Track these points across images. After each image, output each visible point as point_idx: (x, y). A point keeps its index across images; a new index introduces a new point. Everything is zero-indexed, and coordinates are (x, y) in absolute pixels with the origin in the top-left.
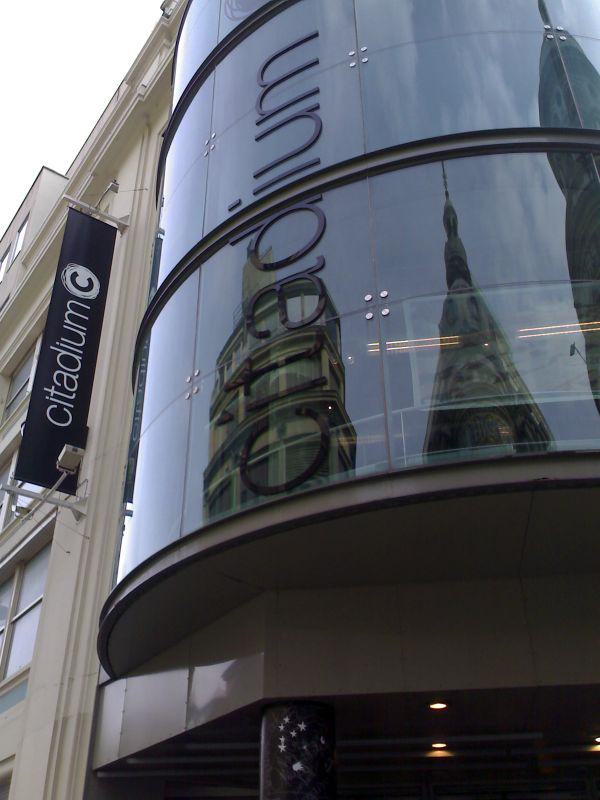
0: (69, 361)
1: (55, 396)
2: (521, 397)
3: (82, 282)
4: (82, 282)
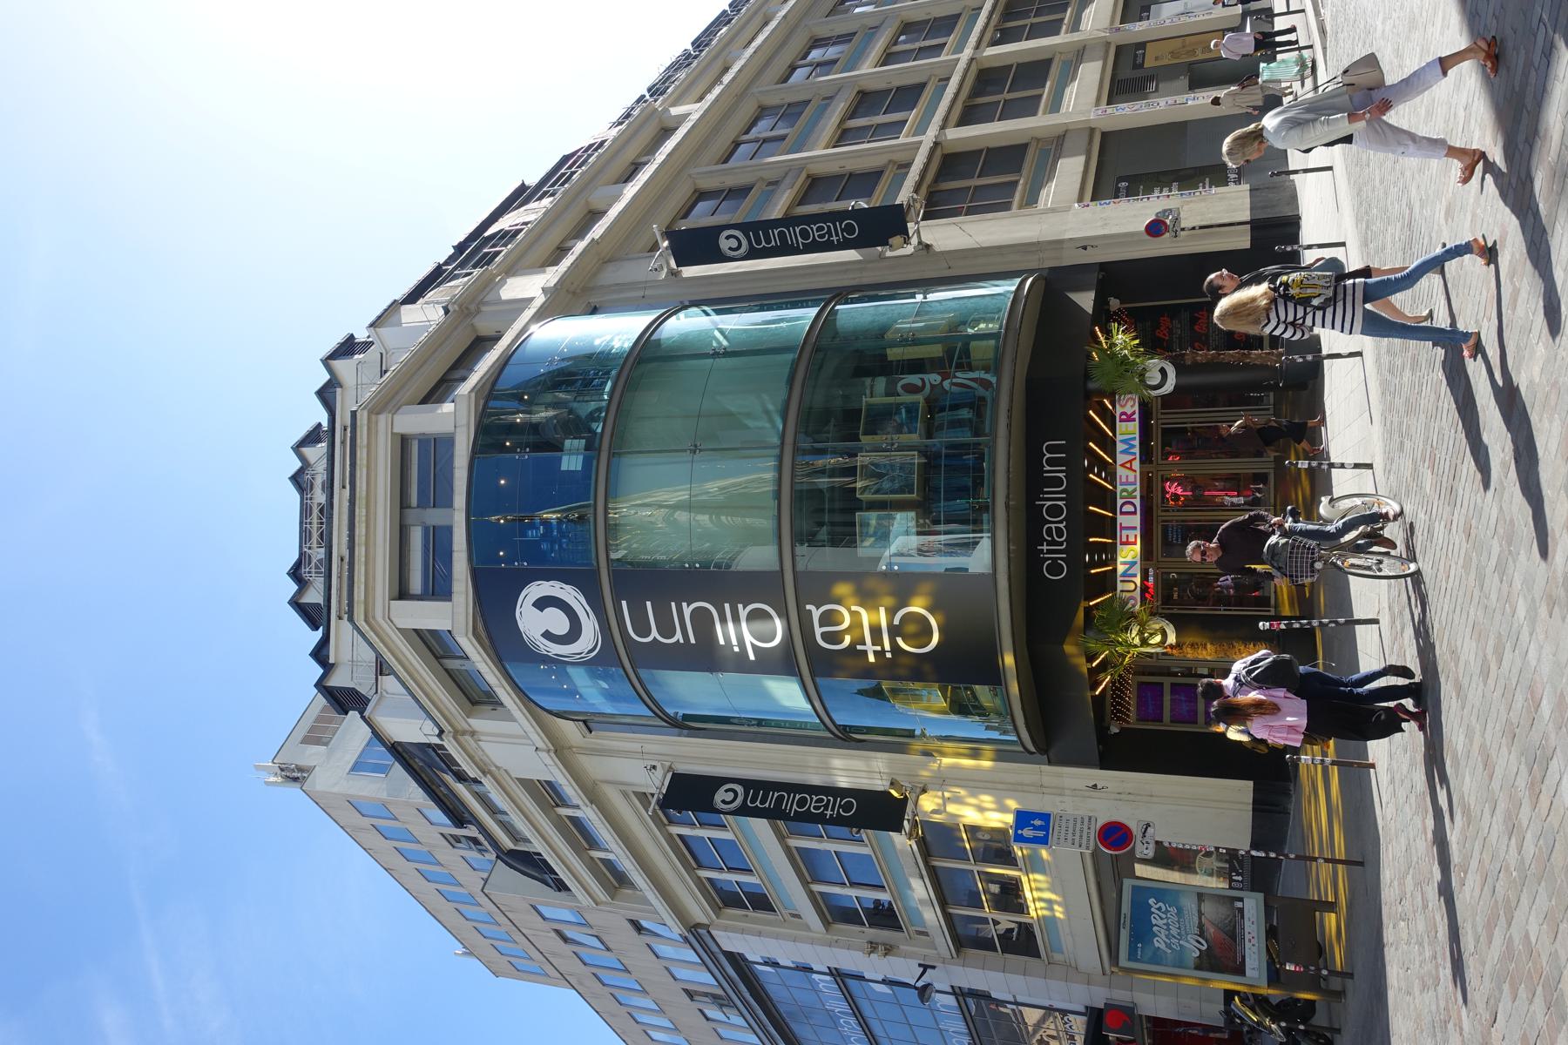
1: (1049, 552)
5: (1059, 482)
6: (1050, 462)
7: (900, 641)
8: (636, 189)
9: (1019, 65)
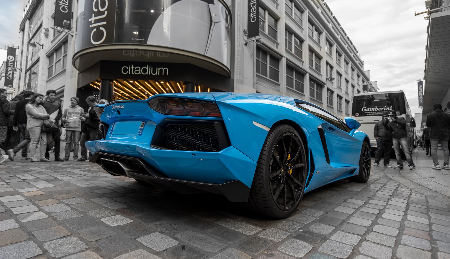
0: (145, 71)
1: (131, 69)
2: (156, 225)
3: (11, 58)
4: (11, 58)
5: (154, 72)
6: (161, 70)
7: (95, 30)
8: (396, 154)
9: (287, 85)
